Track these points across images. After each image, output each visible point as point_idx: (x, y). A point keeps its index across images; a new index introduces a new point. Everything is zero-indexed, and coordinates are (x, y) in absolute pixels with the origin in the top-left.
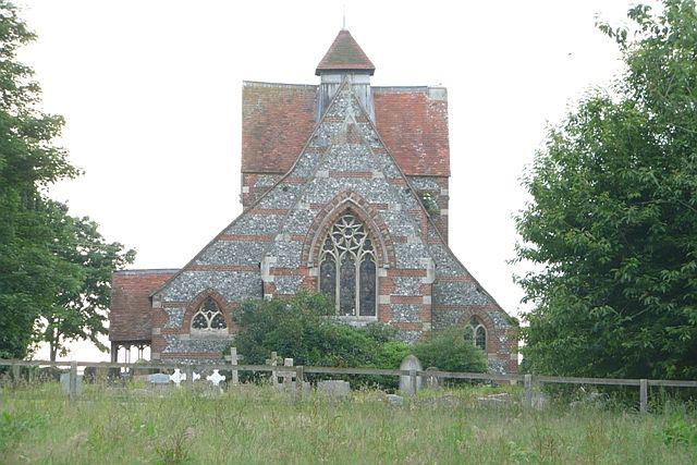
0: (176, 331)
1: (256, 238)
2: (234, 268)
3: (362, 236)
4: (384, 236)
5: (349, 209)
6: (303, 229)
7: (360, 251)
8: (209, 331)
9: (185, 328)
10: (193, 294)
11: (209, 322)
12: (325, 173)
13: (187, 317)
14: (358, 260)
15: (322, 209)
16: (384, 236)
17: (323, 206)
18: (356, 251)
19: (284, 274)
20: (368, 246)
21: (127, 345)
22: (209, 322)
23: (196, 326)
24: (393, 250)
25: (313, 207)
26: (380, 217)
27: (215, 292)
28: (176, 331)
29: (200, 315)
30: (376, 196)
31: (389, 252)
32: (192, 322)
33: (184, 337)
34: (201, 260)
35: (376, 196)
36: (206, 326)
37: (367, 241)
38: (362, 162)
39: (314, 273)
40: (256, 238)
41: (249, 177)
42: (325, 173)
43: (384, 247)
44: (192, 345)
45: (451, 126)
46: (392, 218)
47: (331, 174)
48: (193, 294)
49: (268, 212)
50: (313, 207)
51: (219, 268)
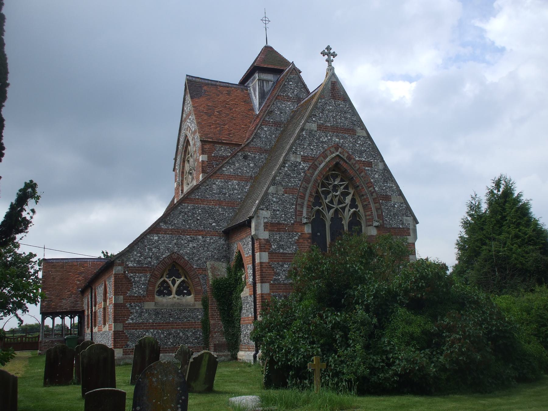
0: (140, 299)
1: (220, 203)
2: (198, 232)
3: (348, 194)
4: (372, 194)
5: (337, 164)
6: (295, 182)
7: (347, 209)
8: (173, 298)
9: (149, 295)
10: (157, 258)
11: (174, 289)
12: (314, 126)
13: (150, 283)
14: (347, 214)
15: (313, 161)
16: (372, 194)
17: (314, 159)
18: (343, 209)
19: (279, 230)
20: (353, 204)
21: (53, 315)
22: (174, 289)
23: (161, 293)
24: (380, 208)
25: (305, 159)
26: (366, 174)
27: (180, 257)
28: (140, 299)
29: (164, 281)
30: (361, 153)
31: (377, 209)
32: (157, 289)
33: (149, 305)
34: (165, 223)
35: (361, 153)
36: (170, 293)
37: (353, 200)
38: (346, 118)
39: (307, 230)
40: (220, 203)
41: (207, 146)
42: (314, 126)
43: (372, 206)
44: (157, 314)
45: (159, 218)
46: (377, 176)
47: (320, 127)
48: (157, 258)
49: (229, 178)
50: (305, 159)
51: (185, 232)
